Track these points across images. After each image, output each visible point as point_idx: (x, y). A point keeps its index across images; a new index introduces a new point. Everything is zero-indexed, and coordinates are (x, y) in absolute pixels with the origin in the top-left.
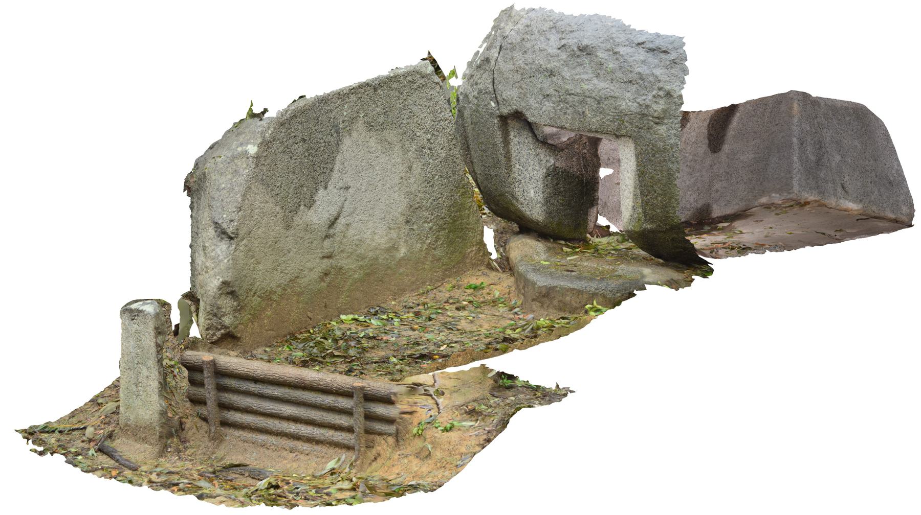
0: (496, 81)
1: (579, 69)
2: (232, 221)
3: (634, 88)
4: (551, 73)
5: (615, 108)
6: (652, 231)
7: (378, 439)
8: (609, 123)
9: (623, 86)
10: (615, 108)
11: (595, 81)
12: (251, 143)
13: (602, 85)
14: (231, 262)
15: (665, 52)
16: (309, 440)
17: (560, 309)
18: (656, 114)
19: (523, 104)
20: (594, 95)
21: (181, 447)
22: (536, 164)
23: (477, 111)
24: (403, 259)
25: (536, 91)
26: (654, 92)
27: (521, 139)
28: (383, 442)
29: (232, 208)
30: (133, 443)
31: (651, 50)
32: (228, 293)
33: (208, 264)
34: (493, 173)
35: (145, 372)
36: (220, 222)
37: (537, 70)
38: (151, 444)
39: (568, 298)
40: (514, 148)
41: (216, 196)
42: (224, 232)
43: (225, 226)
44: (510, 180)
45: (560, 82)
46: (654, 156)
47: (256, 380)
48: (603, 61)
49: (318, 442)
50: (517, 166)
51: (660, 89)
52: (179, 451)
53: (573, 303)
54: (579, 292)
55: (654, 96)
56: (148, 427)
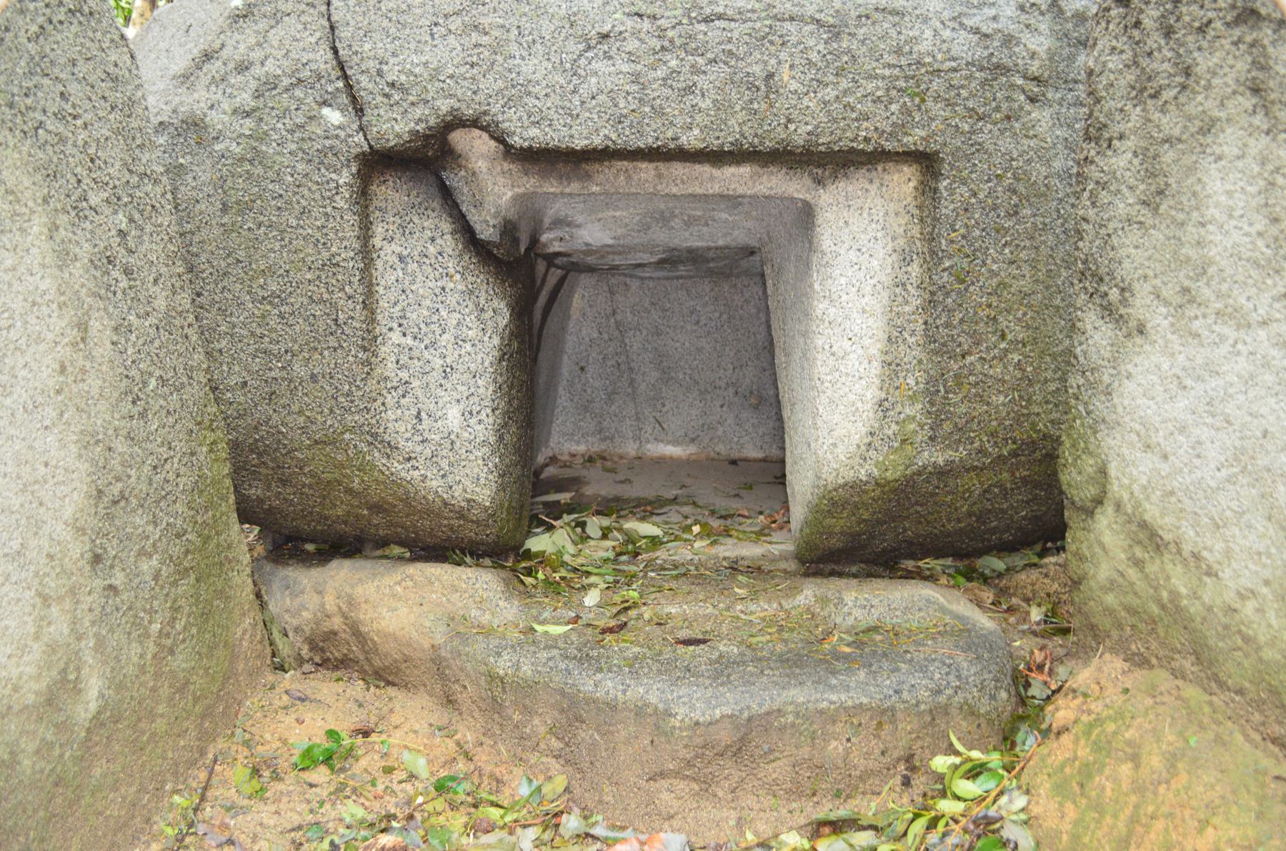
0: (344, 33)
5: (898, 52)
6: (942, 473)
8: (868, 106)
10: (898, 52)
17: (796, 792)
18: (1034, 68)
19: (490, 84)
22: (471, 320)
23: (256, 157)
24: (97, 721)
25: (547, 27)
27: (414, 245)
34: (299, 370)
40: (387, 277)
50: (395, 337)
53: (855, 759)
54: (884, 715)
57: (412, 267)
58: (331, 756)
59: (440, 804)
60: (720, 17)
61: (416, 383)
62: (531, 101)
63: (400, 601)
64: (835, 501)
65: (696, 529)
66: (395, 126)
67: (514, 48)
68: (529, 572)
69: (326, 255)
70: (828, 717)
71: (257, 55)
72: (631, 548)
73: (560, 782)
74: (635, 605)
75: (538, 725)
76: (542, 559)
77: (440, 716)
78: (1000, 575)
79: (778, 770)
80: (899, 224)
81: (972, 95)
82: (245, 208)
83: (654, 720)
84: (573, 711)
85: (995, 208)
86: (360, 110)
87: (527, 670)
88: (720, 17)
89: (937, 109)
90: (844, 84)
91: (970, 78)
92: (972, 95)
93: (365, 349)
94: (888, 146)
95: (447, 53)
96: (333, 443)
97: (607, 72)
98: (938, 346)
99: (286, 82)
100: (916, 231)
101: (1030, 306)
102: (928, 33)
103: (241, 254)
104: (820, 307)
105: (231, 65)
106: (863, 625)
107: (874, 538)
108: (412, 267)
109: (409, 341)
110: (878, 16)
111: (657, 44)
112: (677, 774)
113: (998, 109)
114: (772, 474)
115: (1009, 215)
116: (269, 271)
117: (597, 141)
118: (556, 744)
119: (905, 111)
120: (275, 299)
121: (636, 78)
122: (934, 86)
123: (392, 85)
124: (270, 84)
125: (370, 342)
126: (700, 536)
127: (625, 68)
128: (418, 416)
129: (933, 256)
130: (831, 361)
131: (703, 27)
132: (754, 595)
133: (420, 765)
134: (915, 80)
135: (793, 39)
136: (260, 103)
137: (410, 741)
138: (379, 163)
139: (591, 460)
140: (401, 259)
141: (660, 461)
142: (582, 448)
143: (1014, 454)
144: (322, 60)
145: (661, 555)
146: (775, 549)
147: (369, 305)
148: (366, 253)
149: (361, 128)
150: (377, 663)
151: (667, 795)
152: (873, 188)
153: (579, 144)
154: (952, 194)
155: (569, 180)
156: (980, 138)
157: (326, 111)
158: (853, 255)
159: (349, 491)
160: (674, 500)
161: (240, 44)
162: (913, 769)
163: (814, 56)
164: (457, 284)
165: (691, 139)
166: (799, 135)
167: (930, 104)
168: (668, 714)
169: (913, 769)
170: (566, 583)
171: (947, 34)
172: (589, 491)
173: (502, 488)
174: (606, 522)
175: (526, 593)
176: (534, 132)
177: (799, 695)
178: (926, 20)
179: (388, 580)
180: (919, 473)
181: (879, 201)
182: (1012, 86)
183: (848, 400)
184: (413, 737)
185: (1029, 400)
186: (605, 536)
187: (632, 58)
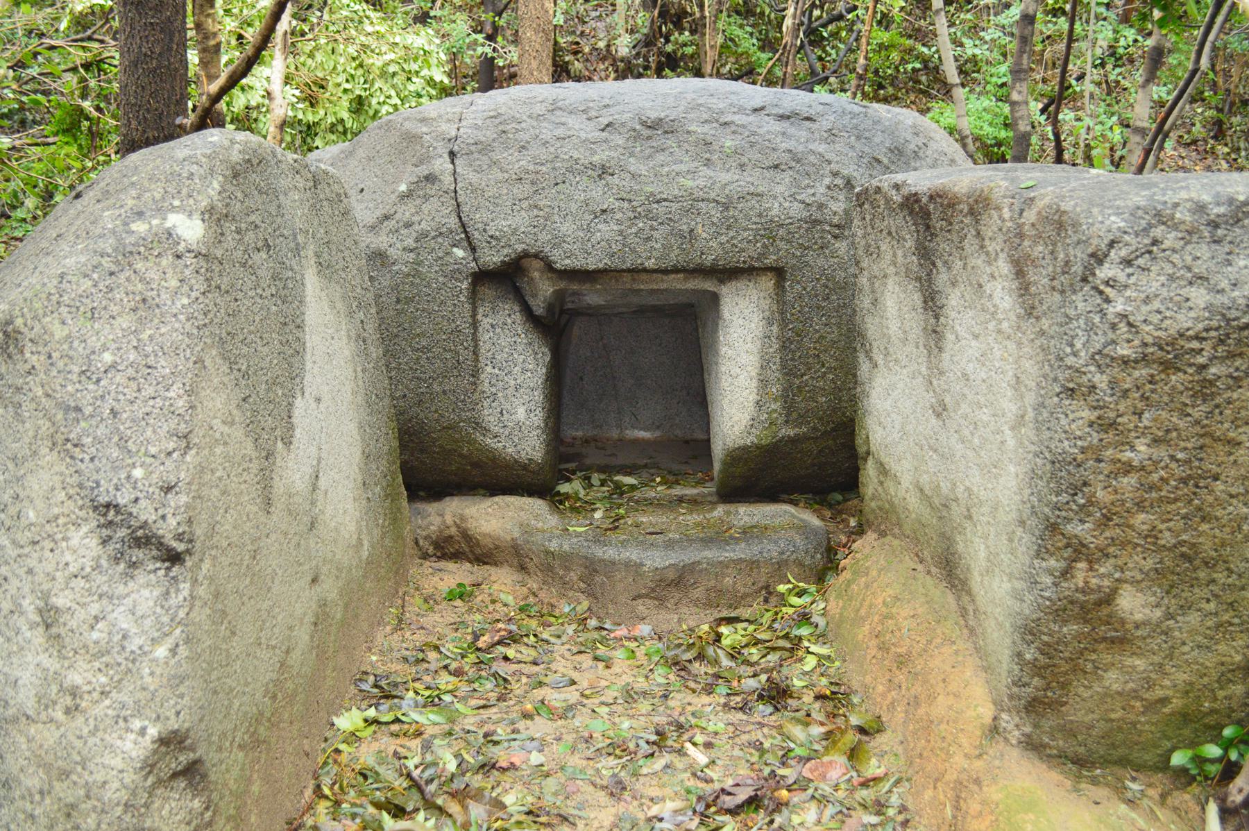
0: (465, 209)
1: (660, 158)
2: (168, 489)
3: (787, 177)
4: (604, 171)
5: (760, 216)
6: (794, 441)
8: (745, 245)
9: (767, 174)
10: (760, 216)
11: (706, 171)
12: (173, 209)
13: (725, 177)
14: (183, 651)
15: (808, 119)
17: (709, 605)
18: (836, 220)
20: (713, 195)
23: (417, 273)
25: (574, 207)
26: (827, 181)
27: (498, 319)
29: (158, 437)
31: (782, 117)
32: (175, 775)
33: (75, 678)
34: (436, 387)
36: (123, 499)
37: (570, 170)
39: (728, 581)
40: (485, 337)
41: (85, 400)
42: (144, 539)
43: (145, 512)
44: (476, 396)
46: (827, 298)
48: (709, 139)
50: (489, 369)
51: (835, 174)
53: (739, 586)
54: (753, 564)
55: (829, 188)
57: (498, 330)
58: (462, 594)
59: (523, 616)
60: (665, 200)
61: (500, 394)
62: (565, 246)
63: (493, 517)
64: (738, 457)
65: (658, 480)
66: (493, 258)
67: (556, 218)
68: (561, 503)
69: (453, 326)
70: (724, 565)
71: (416, 219)
72: (619, 489)
73: (585, 604)
74: (623, 517)
75: (573, 576)
76: (567, 496)
77: (517, 576)
78: (839, 503)
79: (698, 593)
80: (765, 304)
81: (801, 237)
82: (409, 300)
83: (634, 568)
84: (592, 568)
85: (816, 296)
86: (473, 249)
87: (566, 547)
88: (665, 200)
89: (782, 245)
90: (731, 234)
91: (799, 228)
92: (801, 237)
93: (473, 376)
94: (756, 265)
95: (521, 220)
96: (453, 428)
97: (606, 230)
98: (788, 371)
99: (433, 234)
100: (775, 308)
101: (837, 348)
102: (777, 205)
103: (406, 326)
104: (723, 350)
105: (401, 224)
106: (749, 525)
107: (759, 476)
108: (498, 330)
109: (496, 371)
110: (749, 197)
111: (631, 215)
112: (646, 596)
113: (816, 243)
114: (705, 446)
115: (824, 300)
116: (422, 334)
117: (601, 266)
118: (582, 585)
119: (765, 246)
120: (424, 349)
121: (621, 233)
122: (780, 233)
123: (492, 237)
124: (424, 235)
125: (475, 373)
126: (660, 484)
127: (615, 228)
128: (501, 413)
129: (784, 323)
130: (730, 380)
131: (656, 206)
132: (691, 512)
133: (510, 599)
134: (770, 231)
135: (704, 211)
136: (419, 245)
137: (503, 588)
138: (481, 277)
139: (587, 441)
140: (492, 326)
141: (636, 442)
142: (580, 434)
143: (833, 430)
144: (453, 222)
145: (637, 495)
146: (706, 491)
147: (476, 353)
148: (475, 324)
149: (474, 259)
150: (478, 551)
151: (641, 607)
152: (751, 285)
153: (592, 267)
155: (585, 282)
156: (807, 259)
157: (455, 250)
158: (741, 321)
159: (461, 455)
160: (646, 466)
161: (406, 212)
162: (770, 593)
163: (715, 220)
165: (650, 264)
166: (708, 260)
167: (778, 242)
168: (642, 565)
169: (770, 593)
170: (582, 508)
171: (787, 204)
172: (588, 461)
173: (547, 453)
174: (603, 477)
175: (561, 512)
176: (567, 261)
177: (709, 554)
178: (775, 198)
179: (483, 506)
180: (780, 441)
181: (755, 291)
182: (824, 231)
183: (740, 399)
184: (503, 585)
185: (840, 400)
186: (602, 485)
187: (619, 222)
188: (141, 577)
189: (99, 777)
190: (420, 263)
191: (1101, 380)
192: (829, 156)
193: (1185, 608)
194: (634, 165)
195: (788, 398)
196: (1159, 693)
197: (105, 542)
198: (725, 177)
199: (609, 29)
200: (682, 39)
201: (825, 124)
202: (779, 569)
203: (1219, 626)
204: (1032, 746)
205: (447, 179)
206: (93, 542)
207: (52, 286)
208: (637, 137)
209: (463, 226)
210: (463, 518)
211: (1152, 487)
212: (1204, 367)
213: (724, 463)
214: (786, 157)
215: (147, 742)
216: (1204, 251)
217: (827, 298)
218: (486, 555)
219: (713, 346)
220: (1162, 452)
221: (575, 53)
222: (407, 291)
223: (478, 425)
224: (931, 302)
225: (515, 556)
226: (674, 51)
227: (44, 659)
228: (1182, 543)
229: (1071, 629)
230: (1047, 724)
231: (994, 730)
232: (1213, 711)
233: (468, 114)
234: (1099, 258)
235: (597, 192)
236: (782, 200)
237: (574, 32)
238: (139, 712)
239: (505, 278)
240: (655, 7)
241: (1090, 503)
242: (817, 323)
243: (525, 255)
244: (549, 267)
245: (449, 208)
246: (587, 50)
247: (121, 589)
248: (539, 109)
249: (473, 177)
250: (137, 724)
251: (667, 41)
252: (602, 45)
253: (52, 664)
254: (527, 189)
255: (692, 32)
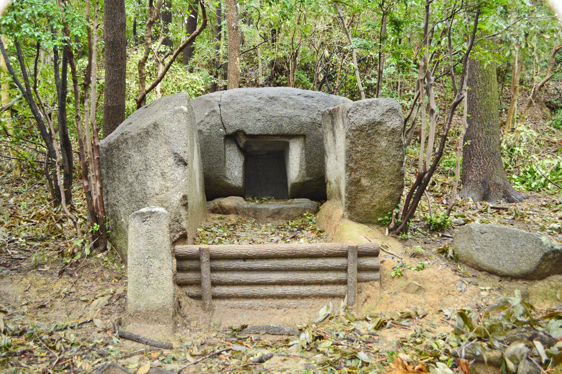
0: (223, 119)
1: (274, 106)
3: (306, 111)
4: (259, 109)
6: (309, 181)
7: (365, 284)
16: (294, 297)
19: (244, 126)
21: (185, 321)
23: (210, 136)
25: (251, 118)
26: (317, 113)
27: (231, 148)
28: (370, 286)
30: (145, 325)
31: (305, 97)
33: (168, 185)
34: (214, 166)
35: (157, 263)
36: (178, 152)
37: (250, 109)
38: (164, 323)
40: (227, 153)
41: (171, 136)
43: (182, 155)
45: (265, 112)
46: (317, 143)
47: (245, 258)
49: (303, 297)
51: (319, 111)
52: (186, 325)
56: (161, 310)
63: (229, 202)
64: (294, 185)
66: (230, 131)
70: (290, 209)
75: (251, 213)
79: (283, 216)
80: (301, 145)
82: (208, 143)
83: (267, 209)
87: (249, 206)
95: (238, 122)
97: (259, 124)
98: (307, 162)
104: (290, 157)
116: (211, 152)
124: (212, 125)
125: (225, 162)
129: (306, 149)
134: (302, 125)
144: (220, 122)
147: (225, 157)
148: (225, 149)
151: (269, 220)
154: (308, 141)
161: (207, 120)
164: (237, 154)
165: (271, 133)
183: (295, 169)
184: (233, 218)
187: (263, 122)
188: (180, 168)
189: (173, 201)
190: (211, 133)
191: (350, 134)
192: (317, 106)
193: (375, 183)
194: (266, 108)
195: (307, 169)
196: (374, 204)
197: (175, 160)
198: (290, 111)
199: (256, 74)
200: (282, 78)
201: (317, 98)
202: (304, 210)
203: (382, 187)
204: (351, 218)
205: (218, 111)
206: (173, 160)
207: (164, 116)
208: (267, 101)
209: (223, 123)
210: (220, 202)
211: (363, 156)
212: (367, 131)
213: (291, 188)
214: (306, 106)
215: (181, 196)
216: (365, 110)
217: (317, 143)
218: (226, 212)
219: (288, 158)
220: (363, 148)
221: (244, 83)
222: (207, 140)
223: (225, 177)
224: (334, 135)
225: (235, 211)
226: (280, 82)
227: (161, 182)
228: (371, 168)
229: (353, 188)
230: (353, 213)
231: (343, 217)
232: (385, 208)
233: (223, 95)
234: (348, 112)
235: (257, 115)
236: (305, 117)
237: (243, 75)
238: (179, 191)
239: (233, 137)
240: (273, 67)
241: (352, 159)
242: (315, 150)
243: (239, 131)
244: (245, 134)
245: (219, 119)
246: (248, 82)
247: (176, 169)
248: (242, 94)
249: (225, 111)
250: (179, 193)
251: (277, 79)
252: (254, 80)
253: (164, 183)
254: (239, 114)
255: (286, 76)
